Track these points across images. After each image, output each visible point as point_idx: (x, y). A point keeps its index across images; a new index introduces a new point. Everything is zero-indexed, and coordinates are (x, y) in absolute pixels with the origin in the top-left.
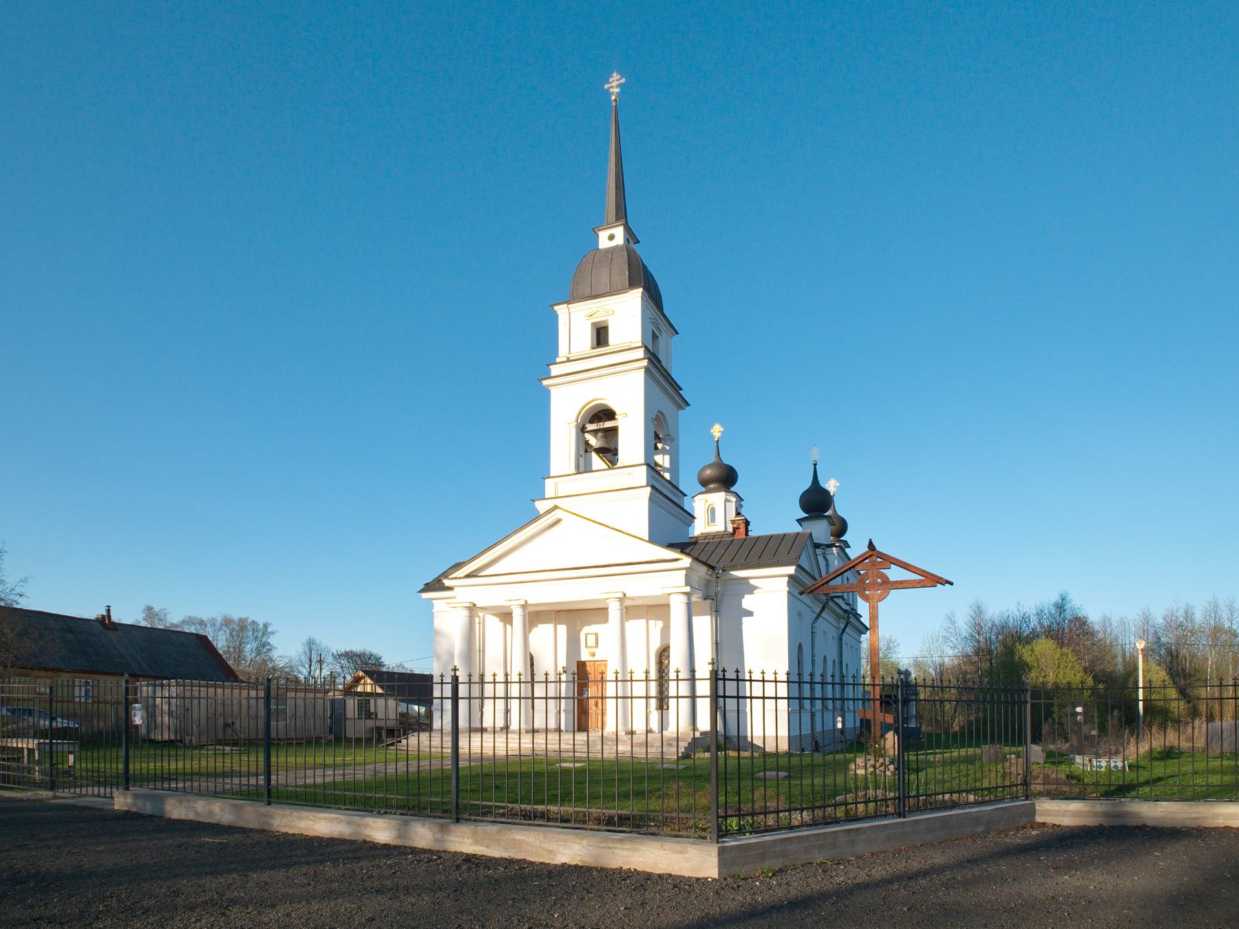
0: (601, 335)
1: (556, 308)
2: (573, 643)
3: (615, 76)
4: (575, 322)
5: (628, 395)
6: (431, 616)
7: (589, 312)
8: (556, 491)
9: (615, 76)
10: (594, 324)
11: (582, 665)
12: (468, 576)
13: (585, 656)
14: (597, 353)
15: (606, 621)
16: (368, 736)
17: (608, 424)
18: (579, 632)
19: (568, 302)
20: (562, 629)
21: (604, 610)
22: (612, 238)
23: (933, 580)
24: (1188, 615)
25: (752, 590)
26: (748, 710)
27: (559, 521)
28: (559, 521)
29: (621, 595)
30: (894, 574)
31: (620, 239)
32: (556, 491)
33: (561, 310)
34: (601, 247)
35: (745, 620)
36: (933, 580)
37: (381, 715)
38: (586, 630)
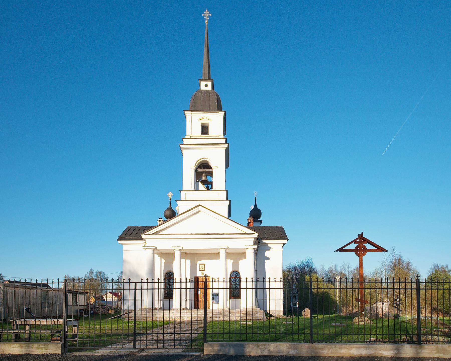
0: (205, 129)
1: (186, 112)
2: (193, 268)
3: (207, 12)
4: (194, 120)
5: (217, 159)
6: (122, 252)
7: (200, 117)
8: (186, 198)
9: (207, 12)
10: (202, 123)
11: (197, 278)
12: (154, 234)
13: (199, 274)
14: (203, 137)
15: (245, 257)
16: (75, 314)
17: (208, 170)
18: (196, 263)
19: (192, 111)
20: (189, 261)
21: (218, 254)
22: (206, 86)
23: (341, 250)
24: (336, 268)
25: (269, 249)
26: (188, 302)
27: (200, 211)
28: (200, 211)
29: (154, 248)
30: (368, 246)
31: (209, 88)
32: (186, 198)
33: (188, 114)
34: (201, 89)
35: (266, 261)
36: (341, 250)
37: (81, 303)
38: (199, 262)
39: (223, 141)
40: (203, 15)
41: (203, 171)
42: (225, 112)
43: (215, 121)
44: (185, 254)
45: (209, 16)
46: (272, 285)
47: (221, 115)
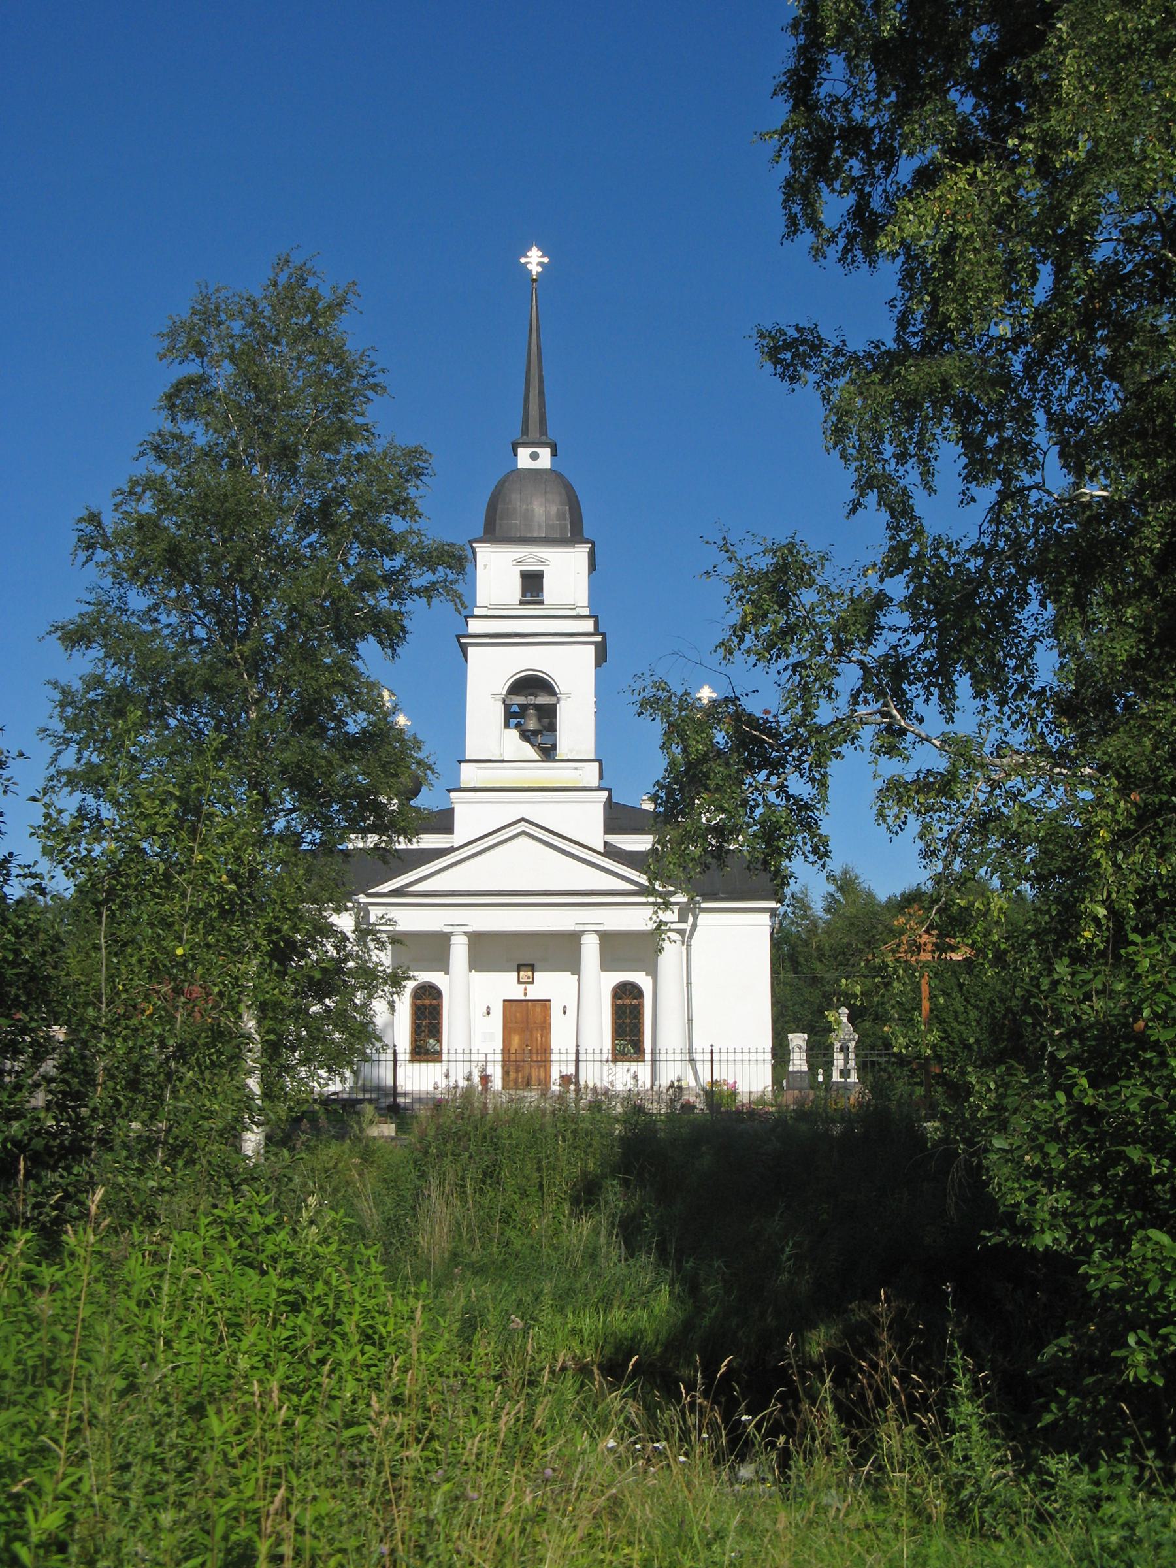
0: (532, 583)
5: (573, 673)
9: (535, 269)
17: (543, 700)
21: (637, 1052)
39: (589, 626)
40: (523, 260)
41: (532, 707)
42: (593, 543)
43: (567, 571)
44: (489, 951)
45: (540, 264)
46: (590, 1057)
47: (578, 556)
